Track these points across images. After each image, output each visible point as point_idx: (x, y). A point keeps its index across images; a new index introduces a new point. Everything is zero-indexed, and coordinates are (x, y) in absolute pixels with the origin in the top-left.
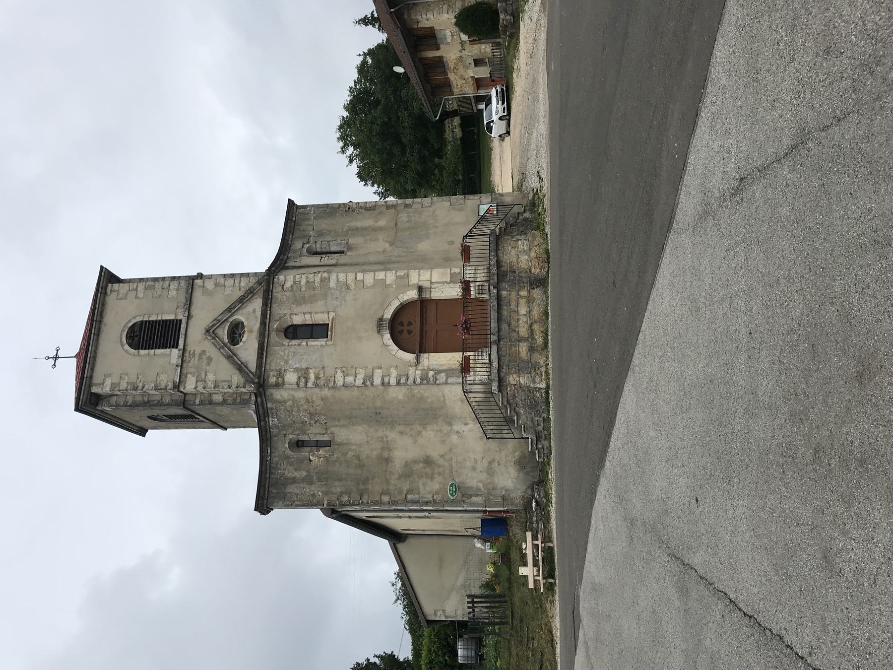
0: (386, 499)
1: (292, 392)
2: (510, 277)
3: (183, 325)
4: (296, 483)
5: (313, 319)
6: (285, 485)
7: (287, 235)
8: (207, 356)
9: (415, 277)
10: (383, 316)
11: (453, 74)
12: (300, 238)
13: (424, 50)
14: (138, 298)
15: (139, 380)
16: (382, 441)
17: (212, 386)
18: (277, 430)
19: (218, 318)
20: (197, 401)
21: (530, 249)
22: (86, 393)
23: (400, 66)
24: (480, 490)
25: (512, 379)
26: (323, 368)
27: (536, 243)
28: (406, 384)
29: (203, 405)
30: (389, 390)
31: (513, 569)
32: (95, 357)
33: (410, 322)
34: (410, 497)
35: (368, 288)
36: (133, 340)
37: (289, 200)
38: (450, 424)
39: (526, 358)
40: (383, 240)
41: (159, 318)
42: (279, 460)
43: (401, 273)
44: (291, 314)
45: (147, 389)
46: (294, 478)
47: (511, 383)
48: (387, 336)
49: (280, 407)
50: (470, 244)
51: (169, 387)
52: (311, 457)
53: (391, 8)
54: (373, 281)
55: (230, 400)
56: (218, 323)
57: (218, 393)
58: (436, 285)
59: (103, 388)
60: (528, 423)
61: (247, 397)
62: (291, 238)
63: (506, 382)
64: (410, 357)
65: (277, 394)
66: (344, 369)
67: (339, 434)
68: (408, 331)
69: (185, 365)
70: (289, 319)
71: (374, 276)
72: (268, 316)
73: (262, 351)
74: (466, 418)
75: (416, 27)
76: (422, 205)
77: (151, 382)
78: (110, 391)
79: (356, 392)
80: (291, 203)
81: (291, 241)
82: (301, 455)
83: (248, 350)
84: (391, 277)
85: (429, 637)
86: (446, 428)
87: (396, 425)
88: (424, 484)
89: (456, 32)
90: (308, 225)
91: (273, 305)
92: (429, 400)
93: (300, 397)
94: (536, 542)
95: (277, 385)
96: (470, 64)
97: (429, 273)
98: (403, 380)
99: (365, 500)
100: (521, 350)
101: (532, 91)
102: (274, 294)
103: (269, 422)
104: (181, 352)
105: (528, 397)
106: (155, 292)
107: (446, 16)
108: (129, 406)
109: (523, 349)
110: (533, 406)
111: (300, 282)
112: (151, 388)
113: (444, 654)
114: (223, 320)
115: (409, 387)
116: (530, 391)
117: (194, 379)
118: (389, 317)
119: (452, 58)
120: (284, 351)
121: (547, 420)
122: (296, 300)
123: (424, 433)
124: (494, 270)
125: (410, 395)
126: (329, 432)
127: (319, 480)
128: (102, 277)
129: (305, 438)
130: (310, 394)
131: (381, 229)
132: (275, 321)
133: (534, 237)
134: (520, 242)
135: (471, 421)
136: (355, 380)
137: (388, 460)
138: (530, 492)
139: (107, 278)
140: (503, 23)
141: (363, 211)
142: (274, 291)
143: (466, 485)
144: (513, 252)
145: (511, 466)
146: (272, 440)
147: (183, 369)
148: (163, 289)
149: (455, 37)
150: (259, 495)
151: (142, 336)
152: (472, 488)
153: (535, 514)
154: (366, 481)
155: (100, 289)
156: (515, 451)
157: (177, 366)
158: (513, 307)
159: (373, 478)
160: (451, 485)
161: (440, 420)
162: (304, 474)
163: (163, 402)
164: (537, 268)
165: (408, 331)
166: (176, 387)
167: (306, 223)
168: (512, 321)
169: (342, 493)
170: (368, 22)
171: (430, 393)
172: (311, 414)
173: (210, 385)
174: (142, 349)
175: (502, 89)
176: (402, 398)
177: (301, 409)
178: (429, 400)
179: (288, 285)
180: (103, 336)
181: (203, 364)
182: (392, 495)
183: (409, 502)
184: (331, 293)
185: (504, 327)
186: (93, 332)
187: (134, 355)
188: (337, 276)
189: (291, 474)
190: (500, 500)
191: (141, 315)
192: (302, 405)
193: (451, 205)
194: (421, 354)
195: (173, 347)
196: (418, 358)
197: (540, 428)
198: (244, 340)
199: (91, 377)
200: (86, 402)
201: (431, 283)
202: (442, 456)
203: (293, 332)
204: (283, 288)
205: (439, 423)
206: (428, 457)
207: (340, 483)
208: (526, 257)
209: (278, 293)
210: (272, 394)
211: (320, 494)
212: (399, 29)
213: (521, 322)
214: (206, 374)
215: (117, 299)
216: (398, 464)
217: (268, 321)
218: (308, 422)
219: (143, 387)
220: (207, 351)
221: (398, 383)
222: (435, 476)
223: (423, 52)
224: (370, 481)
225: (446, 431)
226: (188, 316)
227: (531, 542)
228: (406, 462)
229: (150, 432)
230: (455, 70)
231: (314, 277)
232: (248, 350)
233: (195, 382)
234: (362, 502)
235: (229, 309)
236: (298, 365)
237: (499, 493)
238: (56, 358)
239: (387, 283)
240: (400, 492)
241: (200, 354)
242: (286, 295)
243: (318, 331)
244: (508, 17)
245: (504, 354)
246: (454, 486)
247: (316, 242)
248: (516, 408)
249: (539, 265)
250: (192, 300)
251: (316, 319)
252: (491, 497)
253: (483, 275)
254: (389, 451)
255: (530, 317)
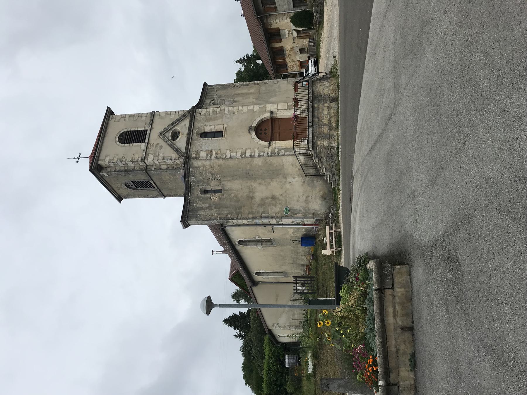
0: (250, 216)
1: (203, 162)
2: (319, 98)
3: (148, 132)
4: (203, 210)
5: (215, 128)
6: (197, 211)
7: (203, 97)
8: (160, 146)
9: (269, 108)
10: (252, 125)
11: (288, 58)
12: (209, 99)
13: (273, 42)
14: (126, 121)
15: (124, 157)
16: (249, 188)
17: (162, 159)
18: (194, 183)
19: (167, 128)
20: (153, 169)
21: (330, 86)
22: (95, 164)
23: (261, 60)
24: (301, 210)
25: (320, 143)
26: (220, 149)
27: (332, 83)
28: (263, 156)
29: (156, 170)
30: (254, 159)
31: (318, 261)
32: (101, 147)
33: (265, 129)
34: (263, 215)
35: (244, 113)
36: (122, 140)
37: (205, 82)
38: (286, 178)
39: (327, 133)
40: (252, 98)
41: (136, 129)
42: (194, 199)
43: (262, 106)
44: (204, 126)
45: (128, 161)
46: (203, 207)
47: (319, 145)
48: (254, 134)
49: (196, 170)
50: (298, 98)
51: (139, 160)
52: (211, 197)
53: (257, 16)
54: (247, 110)
55: (170, 168)
56: (166, 130)
57: (164, 165)
58: (280, 111)
59: (104, 162)
60: (328, 166)
61: (179, 166)
62: (204, 99)
63: (316, 145)
64: (266, 143)
65: (195, 163)
66: (231, 150)
67: (227, 185)
68: (264, 133)
69: (148, 150)
70: (203, 128)
71: (248, 108)
72: (192, 127)
73: (189, 142)
74: (294, 174)
75: (270, 28)
76: (273, 83)
77: (130, 158)
78: (108, 163)
79: (236, 161)
80: (205, 84)
81: (205, 100)
82: (206, 196)
83: (181, 143)
84: (256, 108)
85: (269, 355)
86: (283, 180)
87: (257, 179)
88: (271, 209)
89: (291, 31)
90: (214, 93)
91: (195, 122)
92: (275, 165)
93: (207, 165)
94: (331, 231)
95: (196, 158)
96: (297, 52)
97: (276, 105)
98: (261, 154)
99: (239, 217)
100: (324, 129)
101: (331, 27)
102: (196, 117)
103: (190, 179)
104: (146, 144)
105: (328, 152)
106: (134, 118)
107: (286, 20)
108: (117, 172)
109: (326, 129)
110: (330, 157)
111: (209, 111)
112: (130, 161)
113: (277, 365)
114: (169, 129)
115: (265, 158)
116: (329, 148)
117: (153, 156)
118: (255, 125)
119: (288, 48)
120: (200, 142)
121: (337, 165)
122: (207, 120)
123: (272, 183)
124: (311, 95)
125: (265, 163)
126: (221, 184)
127: (215, 208)
128: (108, 111)
129: (208, 188)
130: (212, 163)
131: (251, 93)
132: (196, 129)
133: (332, 81)
134: (324, 83)
135: (297, 176)
136: (236, 155)
137: (252, 198)
138: (328, 211)
139: (109, 113)
140: (315, 19)
141: (242, 86)
142: (196, 116)
143: (294, 209)
144: (321, 88)
145: (318, 198)
146: (191, 189)
147: (147, 152)
148: (139, 116)
149: (290, 34)
150: (183, 215)
151: (126, 138)
152: (297, 210)
153: (331, 219)
154: (240, 208)
155: (106, 117)
156: (320, 191)
157: (144, 150)
158: (320, 111)
159: (244, 206)
160: (285, 209)
161: (281, 175)
162: (207, 205)
163: (135, 170)
164: (333, 94)
165: (264, 133)
166: (143, 160)
167: (213, 92)
168: (320, 117)
169: (227, 214)
170: (241, 62)
171: (275, 161)
172: (212, 174)
173: (161, 158)
174: (126, 143)
175: (315, 60)
176: (261, 164)
177: (207, 171)
178: (275, 165)
179: (203, 113)
180: (106, 139)
181: (158, 149)
182: (254, 214)
183: (263, 217)
184: (225, 116)
185: (316, 120)
186: (101, 136)
187: (122, 146)
188: (229, 108)
189: (201, 205)
190: (312, 215)
191: (126, 129)
192: (208, 169)
193: (288, 82)
194: (272, 142)
195: (142, 142)
196: (270, 144)
197: (334, 169)
198: (179, 138)
199: (99, 157)
200: (95, 168)
201: (277, 110)
202: (281, 195)
203: (204, 135)
204: (200, 115)
205: (280, 178)
206: (274, 196)
207: (226, 209)
208: (328, 89)
209: (198, 117)
210: (193, 163)
211: (216, 214)
212: (261, 26)
213: (324, 117)
214: (159, 154)
215: (115, 122)
216: (257, 200)
217: (192, 129)
218: (211, 179)
219: (126, 160)
220: (160, 143)
221: (259, 156)
222: (277, 205)
223: (273, 44)
224: (243, 208)
225: (283, 182)
226: (151, 128)
227: (328, 231)
228: (262, 198)
229: (124, 200)
230: (289, 56)
231: (217, 109)
232: (181, 143)
233: (153, 158)
234: (238, 218)
235: (172, 124)
236: (207, 149)
237: (311, 212)
238: (79, 158)
239: (254, 110)
240: (258, 212)
241: (156, 145)
242: (202, 118)
243: (219, 134)
244: (318, 15)
245: (315, 131)
246: (287, 209)
247: (217, 100)
248: (322, 159)
249: (334, 92)
250: (153, 121)
251: (217, 128)
252: (307, 214)
253: (305, 106)
254: (253, 193)
255: (329, 115)
